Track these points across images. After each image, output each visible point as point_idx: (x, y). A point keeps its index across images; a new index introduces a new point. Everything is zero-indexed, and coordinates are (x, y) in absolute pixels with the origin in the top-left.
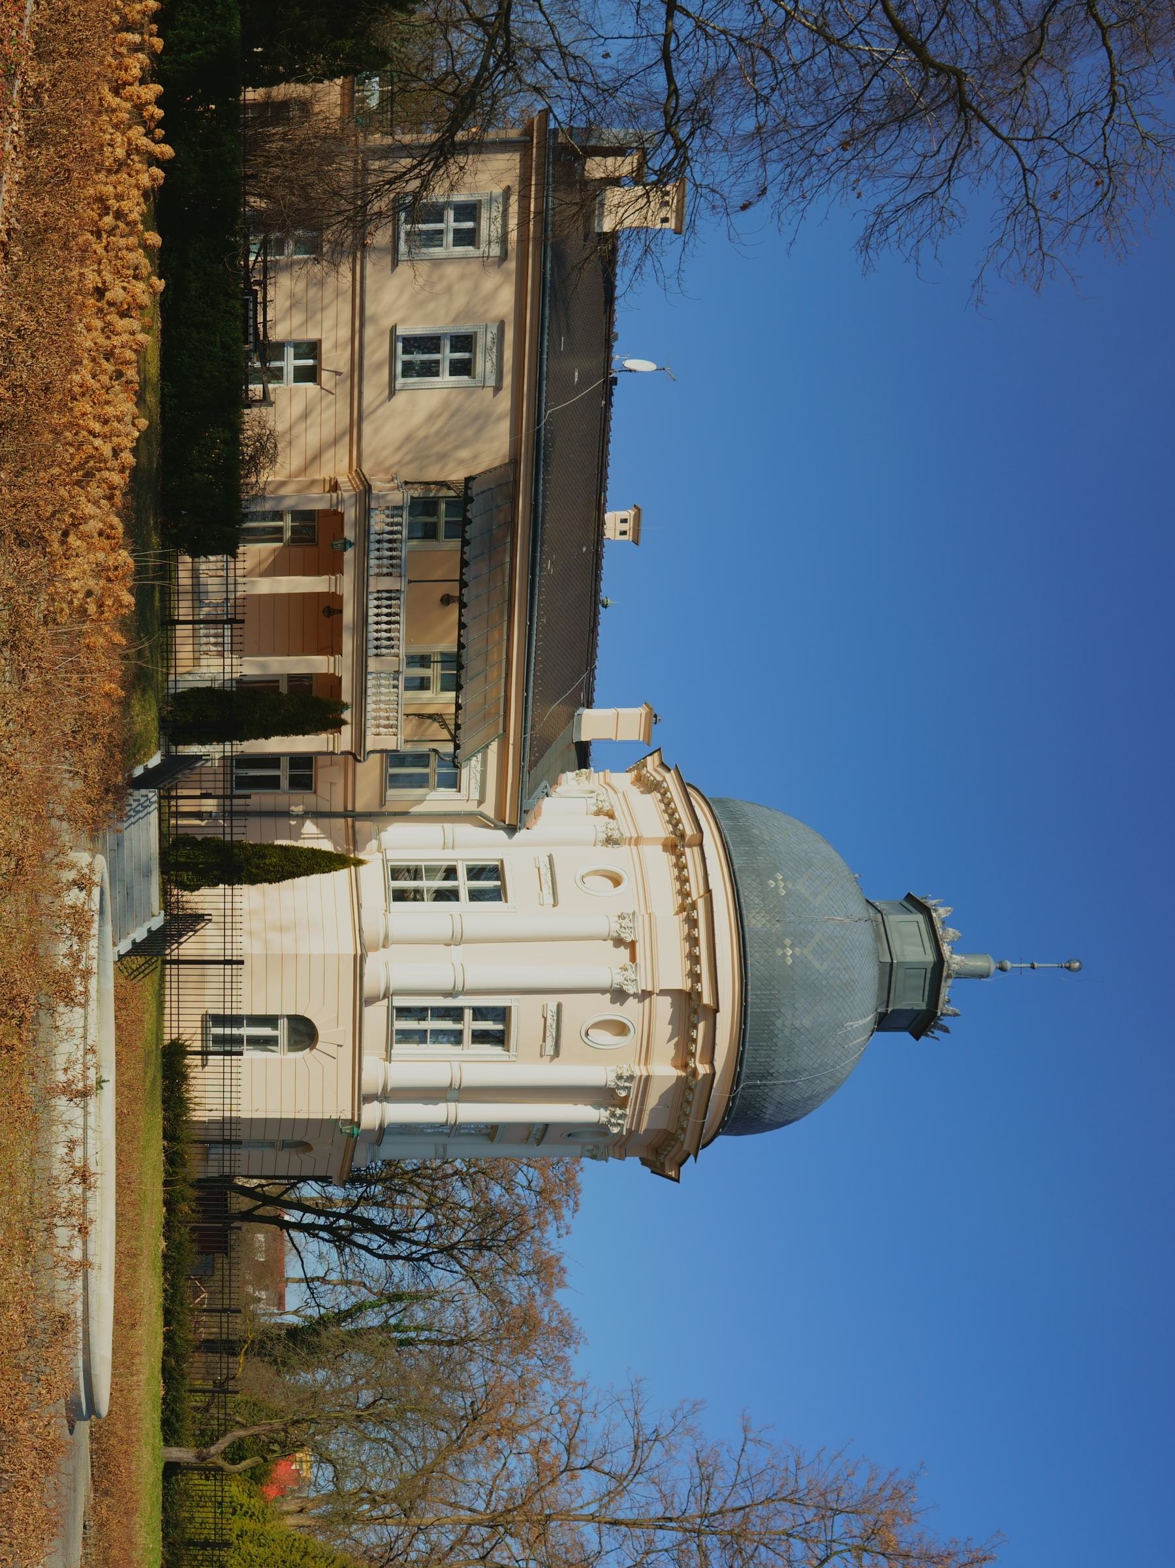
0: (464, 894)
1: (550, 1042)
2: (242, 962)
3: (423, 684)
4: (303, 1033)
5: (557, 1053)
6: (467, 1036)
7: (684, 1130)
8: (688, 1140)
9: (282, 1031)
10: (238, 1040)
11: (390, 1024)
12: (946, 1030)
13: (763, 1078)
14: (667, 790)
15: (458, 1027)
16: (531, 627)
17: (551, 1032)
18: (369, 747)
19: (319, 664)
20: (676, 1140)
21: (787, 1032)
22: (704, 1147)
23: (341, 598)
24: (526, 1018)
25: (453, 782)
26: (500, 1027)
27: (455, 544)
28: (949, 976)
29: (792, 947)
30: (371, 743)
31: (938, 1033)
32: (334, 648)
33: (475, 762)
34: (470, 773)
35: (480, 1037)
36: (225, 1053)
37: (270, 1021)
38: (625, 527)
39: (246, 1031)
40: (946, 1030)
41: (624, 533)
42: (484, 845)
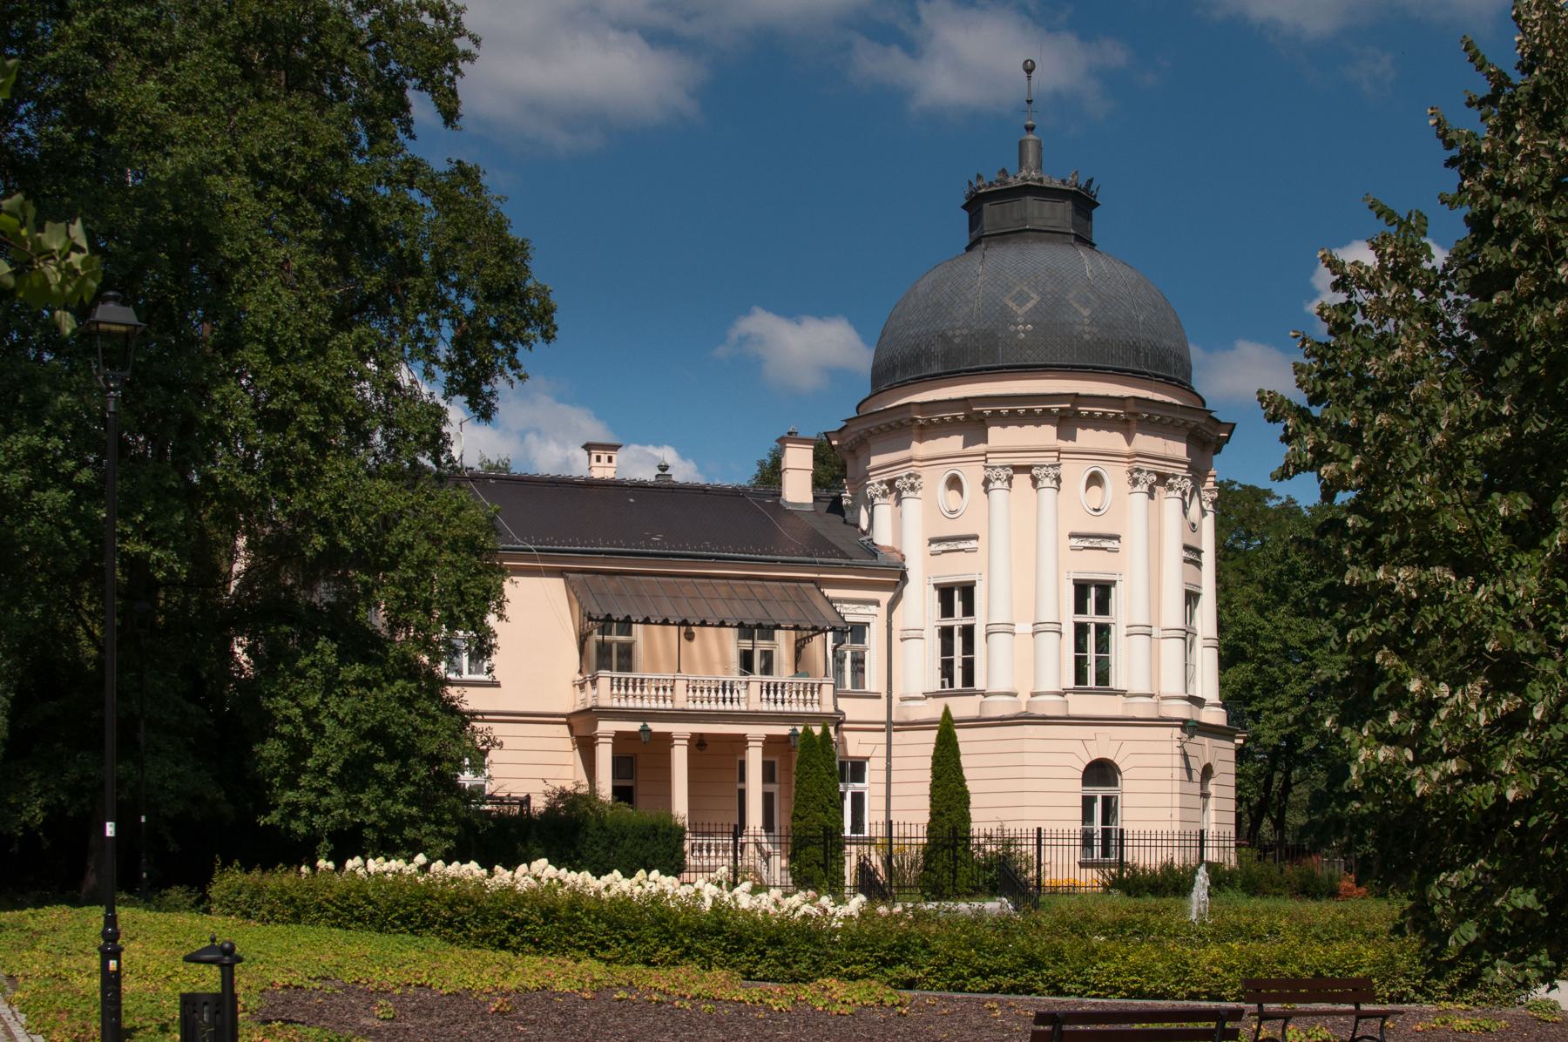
0: (967, 621)
1: (1105, 544)
2: (1039, 830)
3: (768, 656)
4: (1101, 772)
5: (1117, 538)
6: (1102, 619)
7: (1186, 423)
8: (1195, 420)
9: (1099, 792)
10: (1106, 834)
11: (1090, 692)
12: (1090, 181)
13: (1138, 352)
14: (868, 431)
15: (1093, 627)
16: (717, 558)
17: (1096, 543)
18: (831, 709)
19: (754, 760)
20: (1196, 427)
21: (1095, 330)
22: (1204, 403)
23: (618, 733)
24: (1094, 566)
25: (858, 631)
26: (1093, 590)
27: (638, 630)
28: (1041, 180)
29: (1016, 324)
30: (828, 708)
31: (1093, 188)
32: (741, 741)
33: (843, 609)
34: (853, 614)
35: (1103, 607)
36: (1122, 846)
37: (1088, 803)
38: (604, 458)
39: (1098, 825)
40: (1090, 181)
41: (610, 459)
42: (920, 606)
